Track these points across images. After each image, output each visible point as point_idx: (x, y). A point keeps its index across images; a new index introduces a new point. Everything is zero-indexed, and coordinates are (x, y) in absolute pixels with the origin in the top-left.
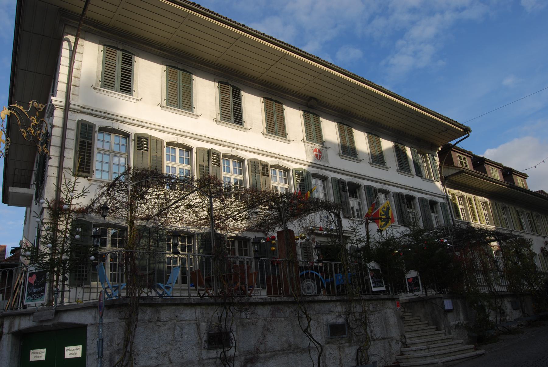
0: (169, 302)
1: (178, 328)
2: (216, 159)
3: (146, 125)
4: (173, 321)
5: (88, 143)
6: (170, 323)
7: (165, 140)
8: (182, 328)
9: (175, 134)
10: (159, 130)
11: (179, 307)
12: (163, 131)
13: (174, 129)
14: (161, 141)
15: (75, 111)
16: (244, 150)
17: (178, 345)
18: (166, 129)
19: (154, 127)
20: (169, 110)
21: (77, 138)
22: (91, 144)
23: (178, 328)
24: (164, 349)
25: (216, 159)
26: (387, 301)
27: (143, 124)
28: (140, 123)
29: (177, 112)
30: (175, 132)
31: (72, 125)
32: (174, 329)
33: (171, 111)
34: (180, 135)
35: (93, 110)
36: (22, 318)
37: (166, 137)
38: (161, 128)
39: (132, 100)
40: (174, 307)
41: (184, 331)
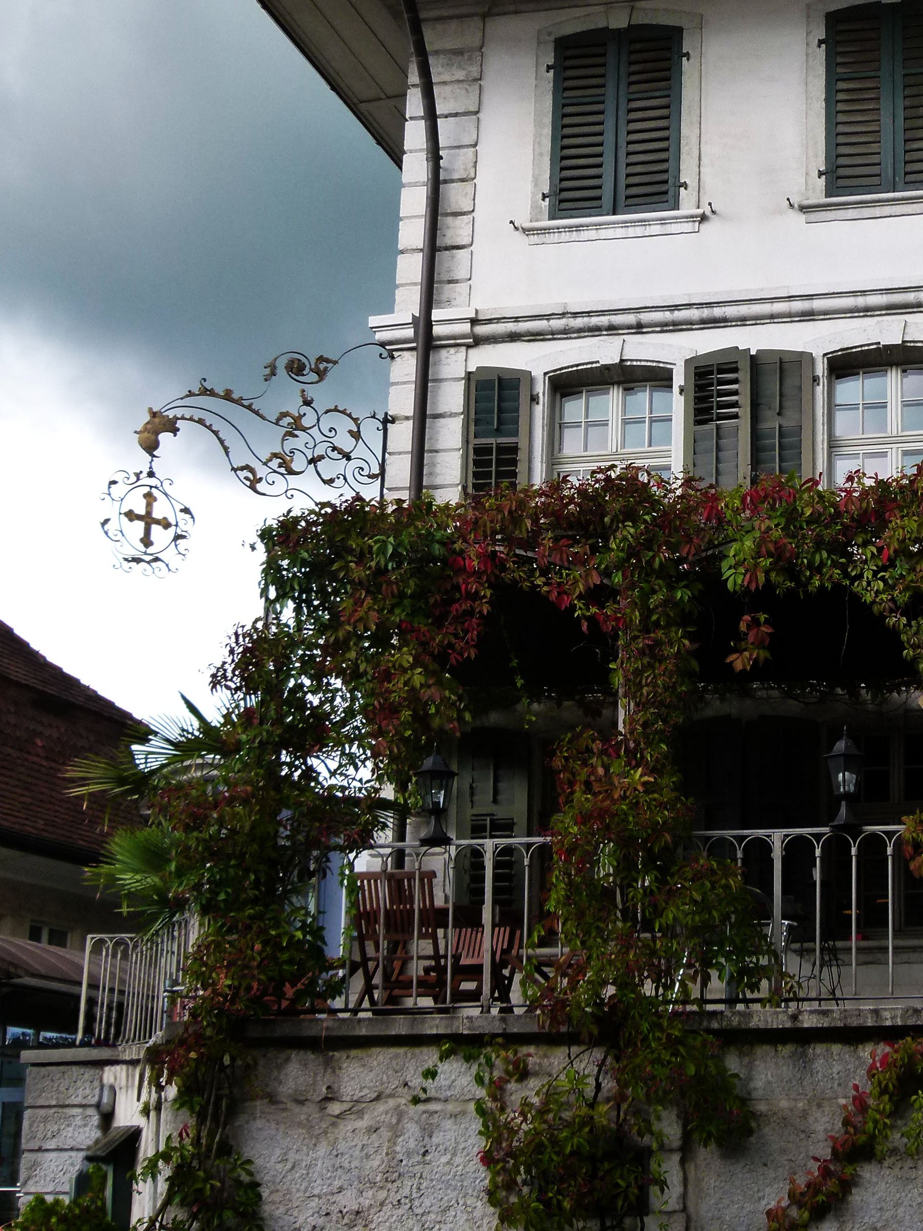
0: (363, 1032)
1: (412, 1130)
2: (721, 394)
3: (730, 311)
4: (391, 1102)
5: (501, 449)
6: (381, 1107)
7: (538, 372)
8: (428, 1131)
9: (612, 329)
10: (790, 317)
11: (417, 1051)
12: (808, 316)
13: (854, 293)
14: (802, 360)
15: (454, 341)
16: (513, 337)
17: (406, 1192)
18: (818, 304)
19: (766, 308)
20: (841, 214)
21: (466, 441)
22: (514, 449)
23: (412, 1130)
24: (349, 1201)
25: (721, 394)
26: (820, 1049)
27: (718, 312)
28: (706, 313)
29: (877, 211)
30: (861, 301)
31: (451, 398)
32: (396, 1132)
33: (851, 213)
34: (891, 309)
35: (516, 319)
36: (762, 1051)
37: (818, 340)
38: (798, 306)
39: (674, 228)
40: (401, 1051)
41: (435, 1140)
